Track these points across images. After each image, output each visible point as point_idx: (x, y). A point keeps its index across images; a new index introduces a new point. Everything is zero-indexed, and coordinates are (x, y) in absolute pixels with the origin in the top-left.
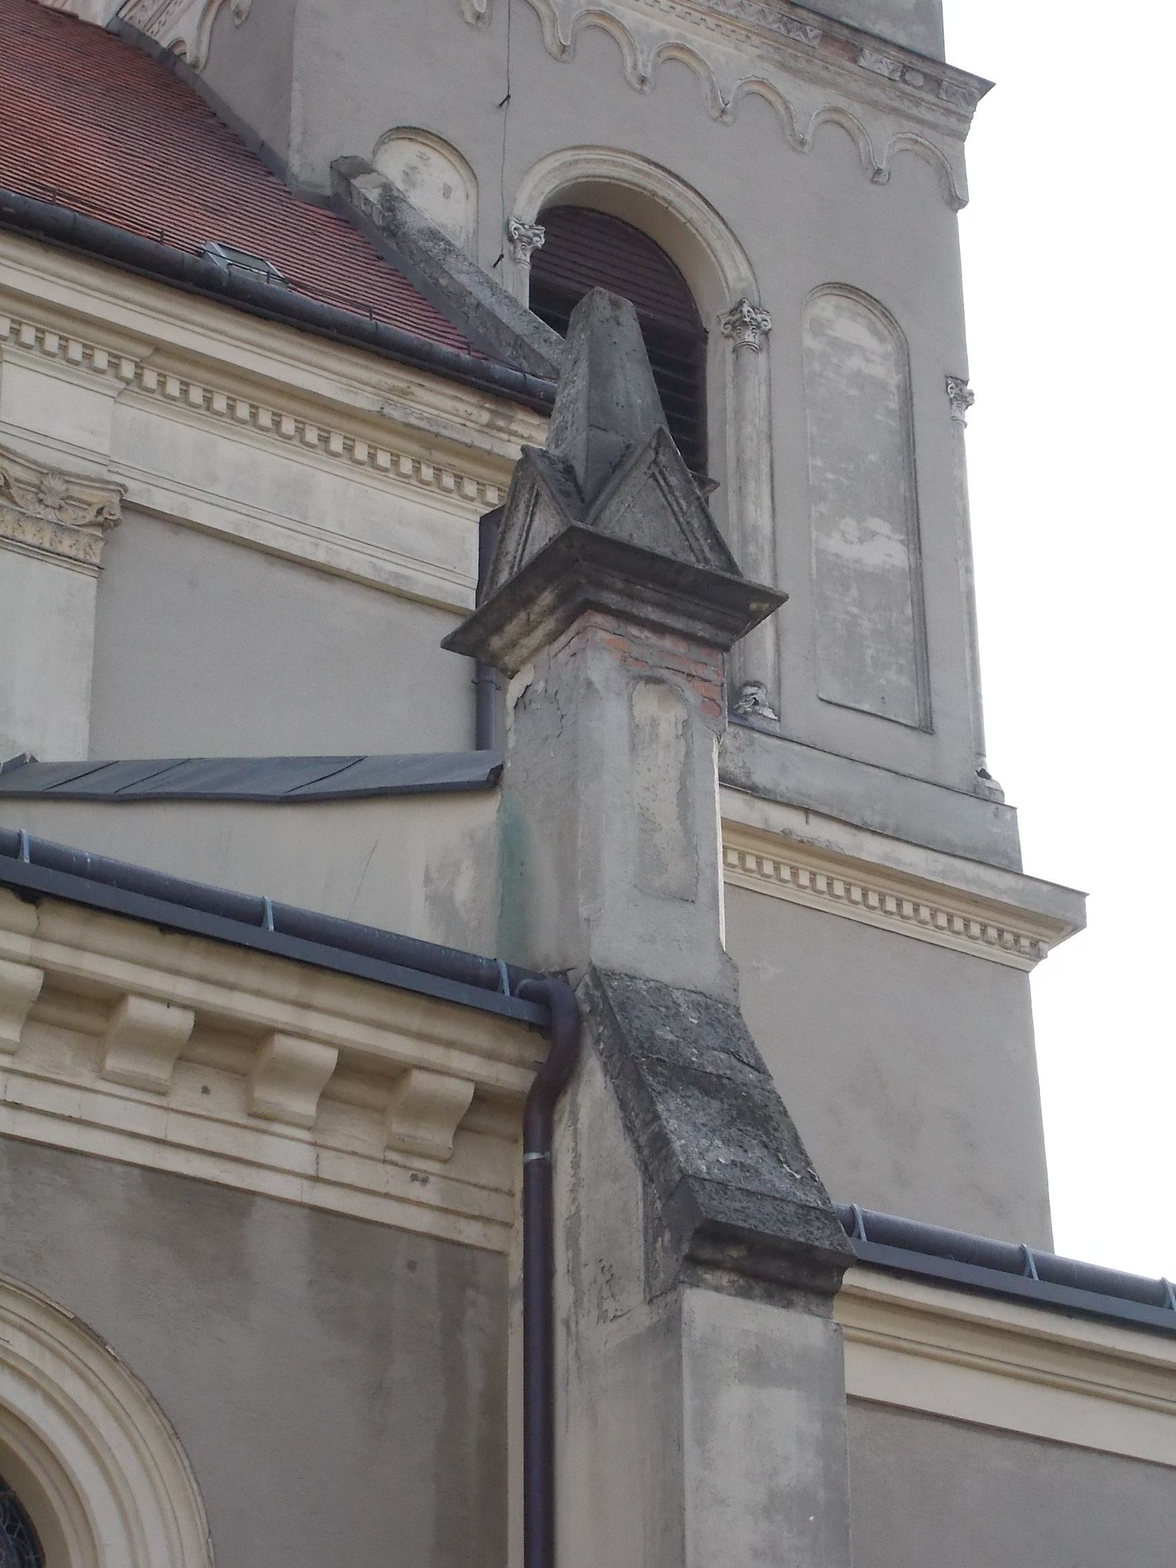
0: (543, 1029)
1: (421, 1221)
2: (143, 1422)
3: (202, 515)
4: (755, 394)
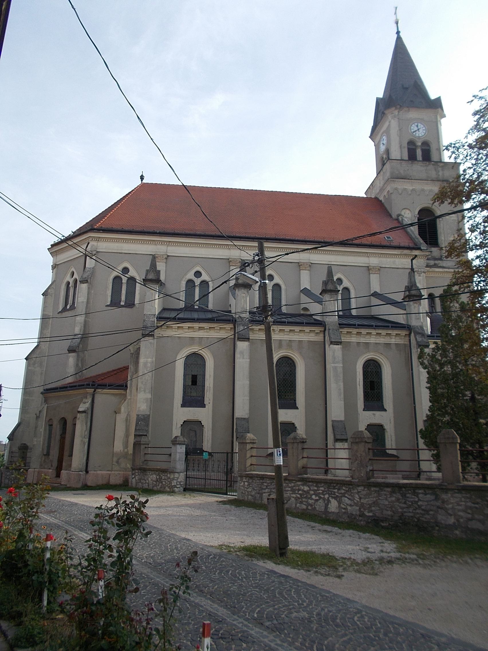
0: (409, 330)
1: (403, 343)
2: (386, 359)
3: (387, 266)
4: (442, 225)
